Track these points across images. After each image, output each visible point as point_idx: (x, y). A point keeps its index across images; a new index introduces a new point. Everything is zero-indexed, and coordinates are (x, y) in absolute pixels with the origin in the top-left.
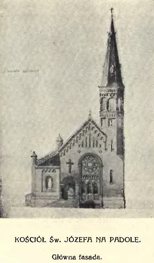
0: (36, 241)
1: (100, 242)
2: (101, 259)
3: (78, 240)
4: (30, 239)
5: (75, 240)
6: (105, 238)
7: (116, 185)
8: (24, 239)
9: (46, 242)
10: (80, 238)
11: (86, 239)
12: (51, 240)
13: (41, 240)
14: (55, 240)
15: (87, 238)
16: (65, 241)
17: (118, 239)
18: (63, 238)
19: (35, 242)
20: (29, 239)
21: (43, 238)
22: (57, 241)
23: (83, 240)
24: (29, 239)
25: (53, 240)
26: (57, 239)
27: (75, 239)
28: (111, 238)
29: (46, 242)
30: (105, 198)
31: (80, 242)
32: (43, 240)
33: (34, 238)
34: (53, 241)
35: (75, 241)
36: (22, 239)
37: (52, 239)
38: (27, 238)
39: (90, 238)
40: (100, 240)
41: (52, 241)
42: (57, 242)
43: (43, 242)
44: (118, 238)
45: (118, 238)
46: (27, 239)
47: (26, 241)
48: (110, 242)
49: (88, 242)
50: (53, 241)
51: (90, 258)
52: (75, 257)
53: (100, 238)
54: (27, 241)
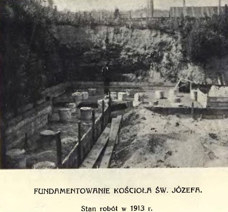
1: (48, 193)
3: (185, 190)
4: (130, 189)
5: (186, 189)
6: (199, 188)
7: (79, 106)
8: (130, 191)
10: (187, 188)
11: (194, 190)
12: (157, 191)
13: (85, 190)
15: (38, 189)
17: (96, 190)
18: (170, 189)
19: (135, 192)
20: (129, 190)
21: (143, 188)
22: (163, 191)
23: (70, 192)
24: (129, 190)
25: (159, 191)
27: (182, 190)
30: (222, 130)
31: (187, 192)
32: (143, 191)
33: (134, 189)
34: (159, 191)
35: (183, 192)
36: (122, 191)
37: (157, 190)
38: (127, 189)
39: (198, 189)
40: (102, 191)
41: (158, 192)
42: (90, 193)
43: (143, 192)
44: (96, 189)
45: (96, 189)
47: (125, 192)
48: (35, 193)
49: (196, 192)
50: (159, 191)
51: (90, 210)
53: (48, 189)
54: (127, 192)
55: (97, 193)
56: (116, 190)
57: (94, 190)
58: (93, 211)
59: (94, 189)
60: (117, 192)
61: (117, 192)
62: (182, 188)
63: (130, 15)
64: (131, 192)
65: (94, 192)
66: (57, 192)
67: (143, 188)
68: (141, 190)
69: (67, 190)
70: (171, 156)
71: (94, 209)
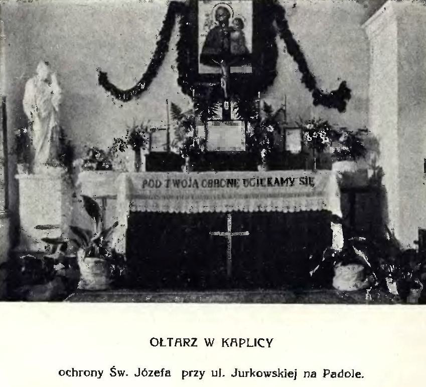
0: (287, 376)
2: (127, 375)
5: (148, 375)
9: (197, 346)
14: (265, 374)
16: (232, 375)
17: (236, 342)
19: (255, 345)
21: (161, 339)
22: (121, 374)
25: (115, 373)
26: (268, 372)
28: (325, 370)
29: (197, 346)
32: (161, 343)
35: (152, 371)
37: (113, 372)
39: (234, 340)
41: (113, 374)
42: (211, 346)
46: (75, 373)
48: (324, 377)
52: (169, 373)
55: (237, 346)
56: (226, 342)
57: (176, 342)
58: (243, 372)
59: (232, 339)
60: (227, 344)
61: (227, 344)
62: (192, 339)
63: (195, 130)
64: (259, 345)
65: (176, 344)
66: (234, 344)
67: (161, 339)
68: (158, 342)
69: (184, 340)
70: (343, 114)
71: (215, 374)
